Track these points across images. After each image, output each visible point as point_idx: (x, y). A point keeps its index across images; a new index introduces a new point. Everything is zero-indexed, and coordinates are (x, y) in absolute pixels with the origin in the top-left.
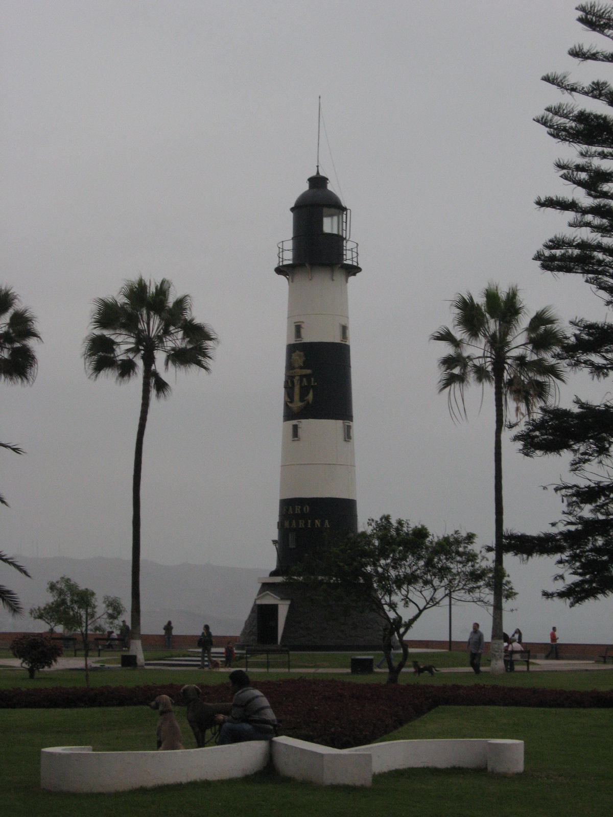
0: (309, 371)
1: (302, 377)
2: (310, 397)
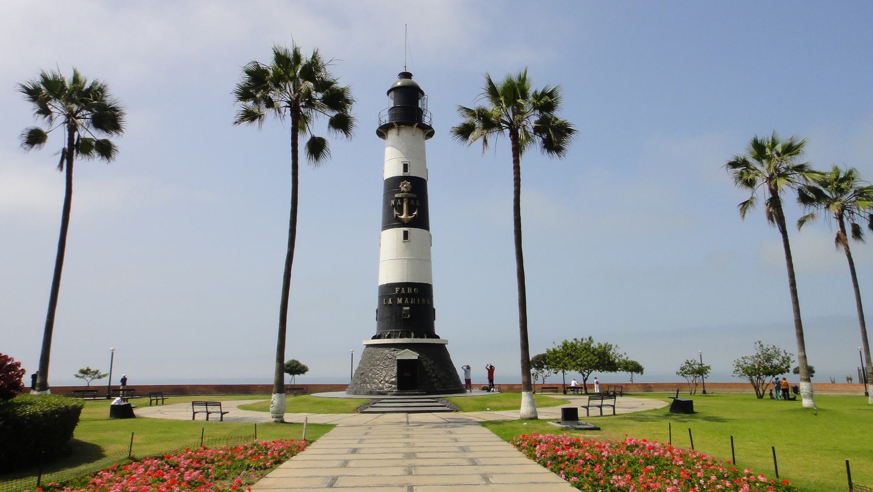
0: (415, 196)
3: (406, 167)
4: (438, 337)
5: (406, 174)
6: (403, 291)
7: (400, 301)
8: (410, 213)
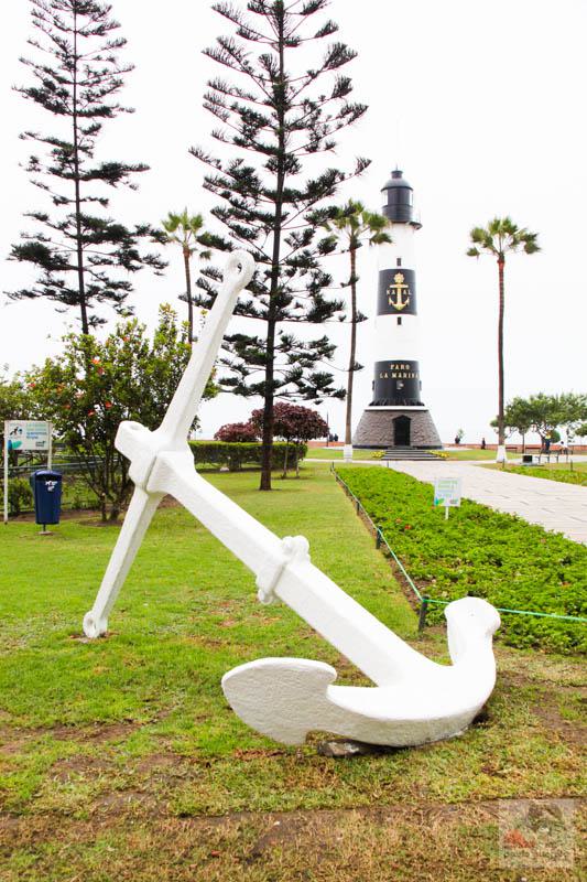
1: (403, 290)
2: (407, 301)
3: (399, 261)
4: (420, 404)
5: (399, 268)
6: (397, 368)
7: (394, 376)
8: (403, 303)
